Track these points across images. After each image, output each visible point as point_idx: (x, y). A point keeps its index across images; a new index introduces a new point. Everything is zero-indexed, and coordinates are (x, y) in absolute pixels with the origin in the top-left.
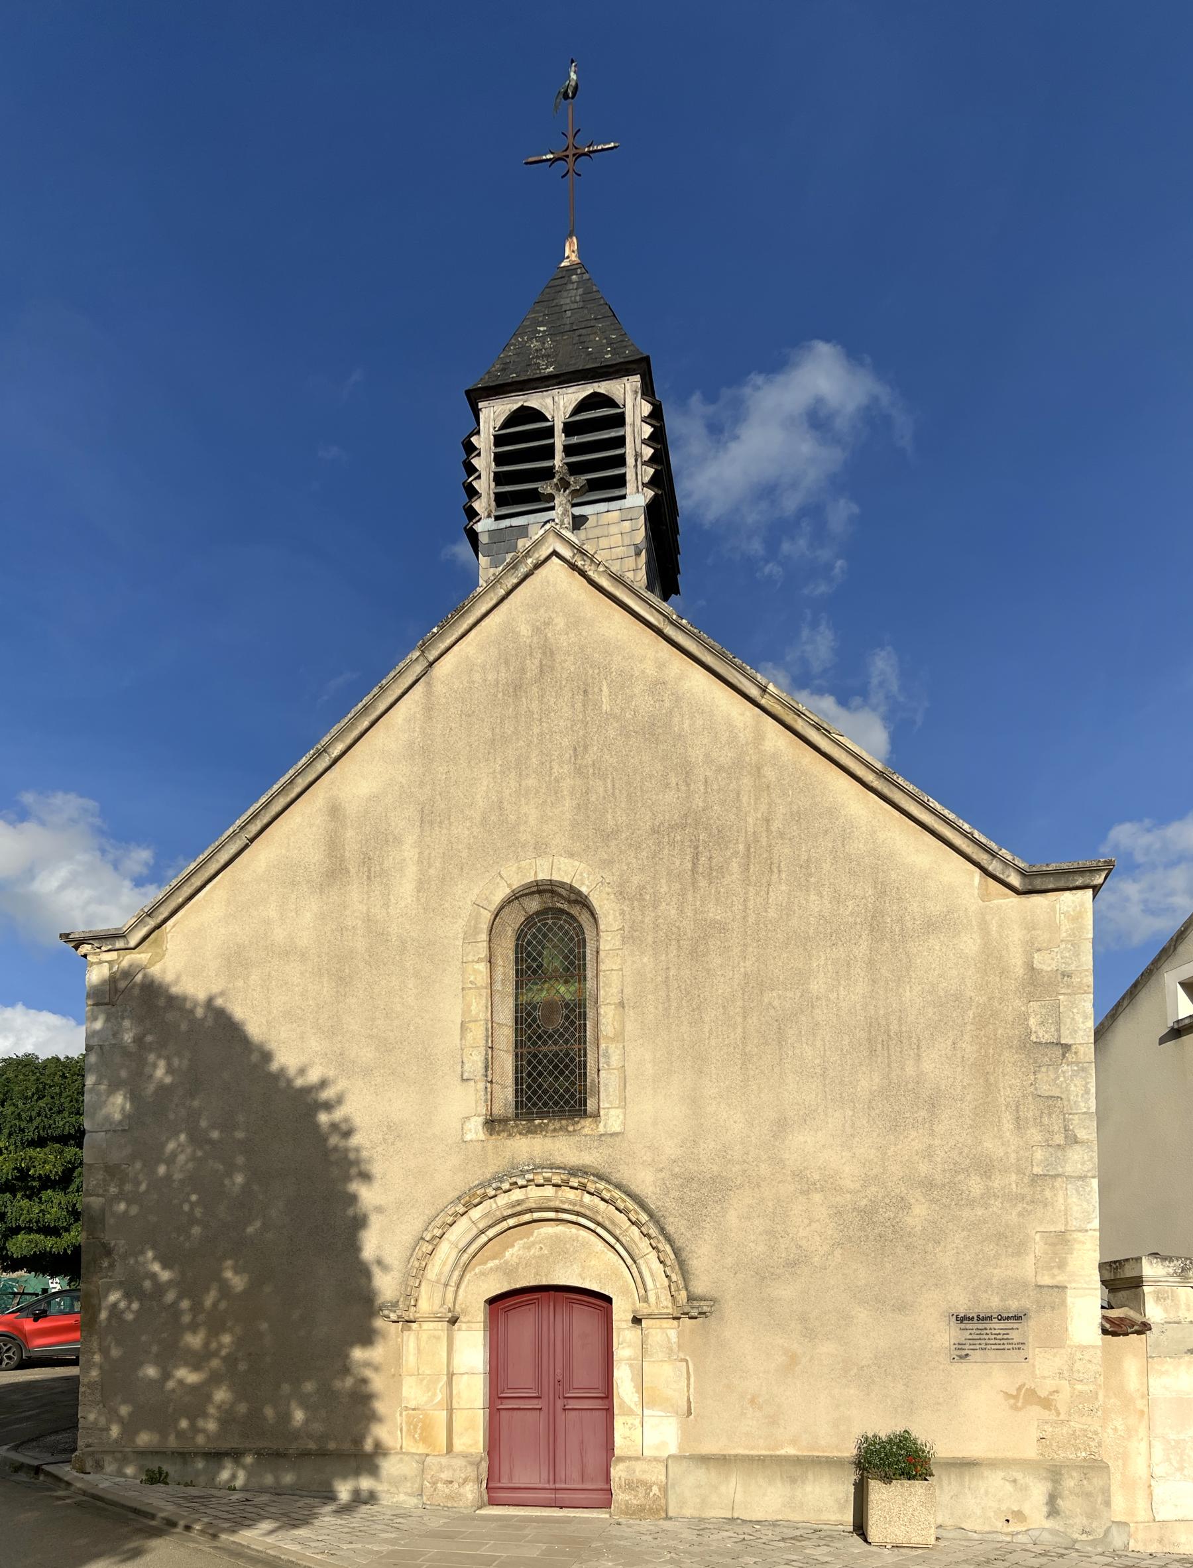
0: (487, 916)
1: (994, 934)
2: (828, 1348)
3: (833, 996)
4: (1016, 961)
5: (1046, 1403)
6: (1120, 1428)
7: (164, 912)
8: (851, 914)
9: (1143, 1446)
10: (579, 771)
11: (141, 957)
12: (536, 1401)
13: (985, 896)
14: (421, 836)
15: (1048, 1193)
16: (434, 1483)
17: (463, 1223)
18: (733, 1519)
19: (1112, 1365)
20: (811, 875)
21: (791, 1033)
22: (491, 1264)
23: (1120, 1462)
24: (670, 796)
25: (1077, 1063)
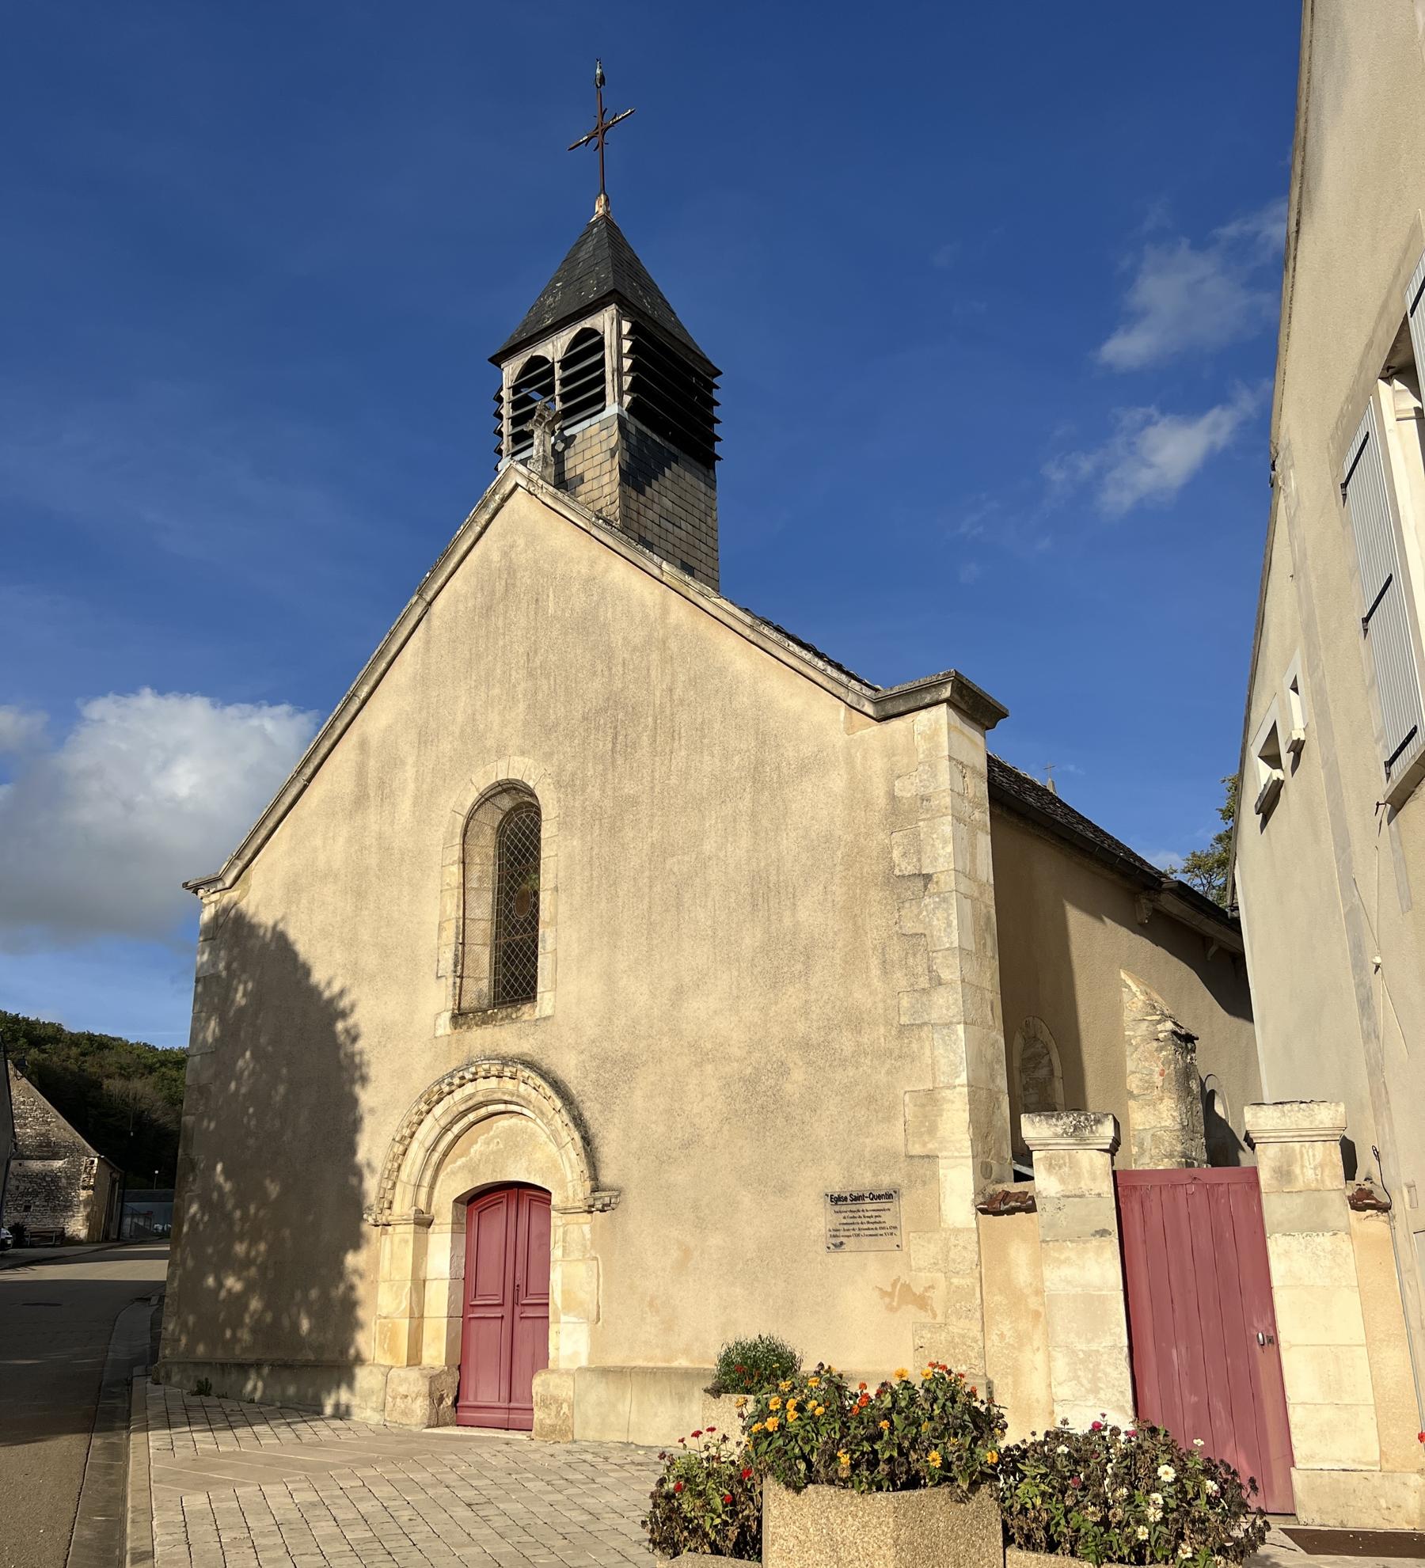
0: (461, 821)
1: (859, 767)
2: (715, 1240)
3: (722, 854)
4: (878, 792)
5: (922, 1302)
6: (1008, 1334)
7: (248, 854)
8: (737, 769)
9: (1039, 1358)
10: (531, 674)
11: (233, 895)
12: (499, 1309)
13: (850, 729)
14: (419, 756)
15: (915, 1046)
16: (394, 1398)
17: (429, 1120)
18: (628, 1444)
19: (990, 1256)
20: (704, 737)
21: (687, 897)
22: (459, 1162)
23: (1010, 1380)
24: (596, 684)
25: (938, 894)
